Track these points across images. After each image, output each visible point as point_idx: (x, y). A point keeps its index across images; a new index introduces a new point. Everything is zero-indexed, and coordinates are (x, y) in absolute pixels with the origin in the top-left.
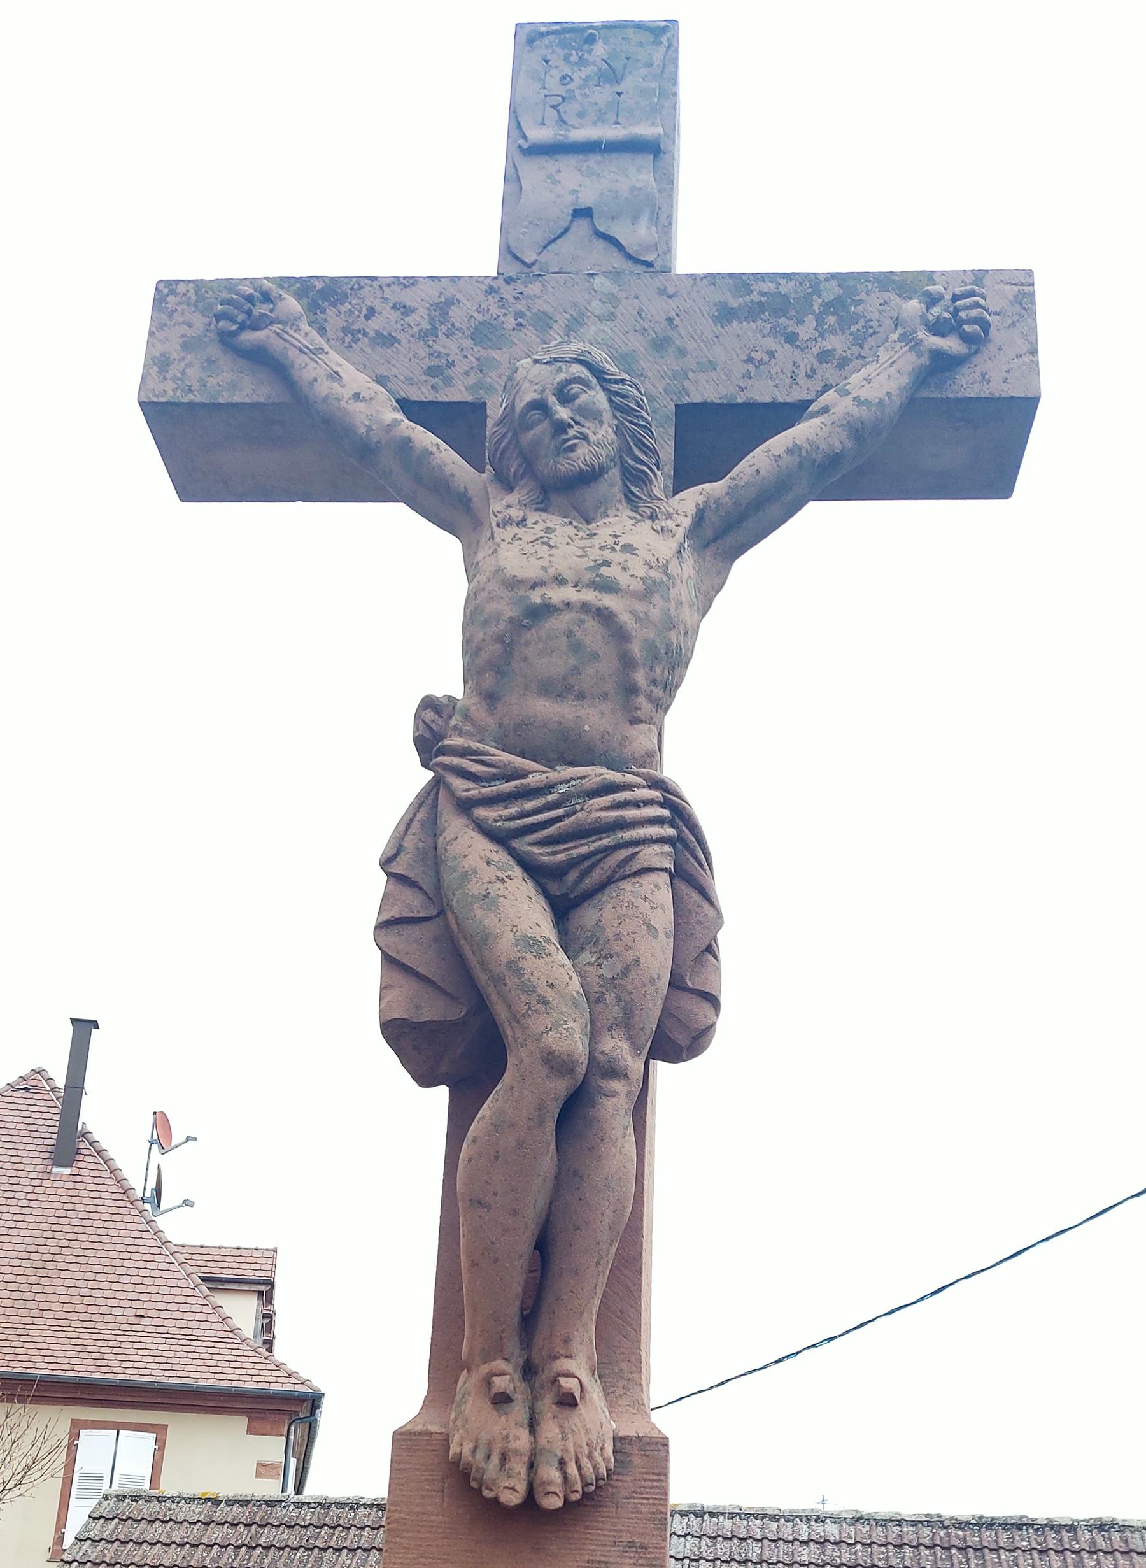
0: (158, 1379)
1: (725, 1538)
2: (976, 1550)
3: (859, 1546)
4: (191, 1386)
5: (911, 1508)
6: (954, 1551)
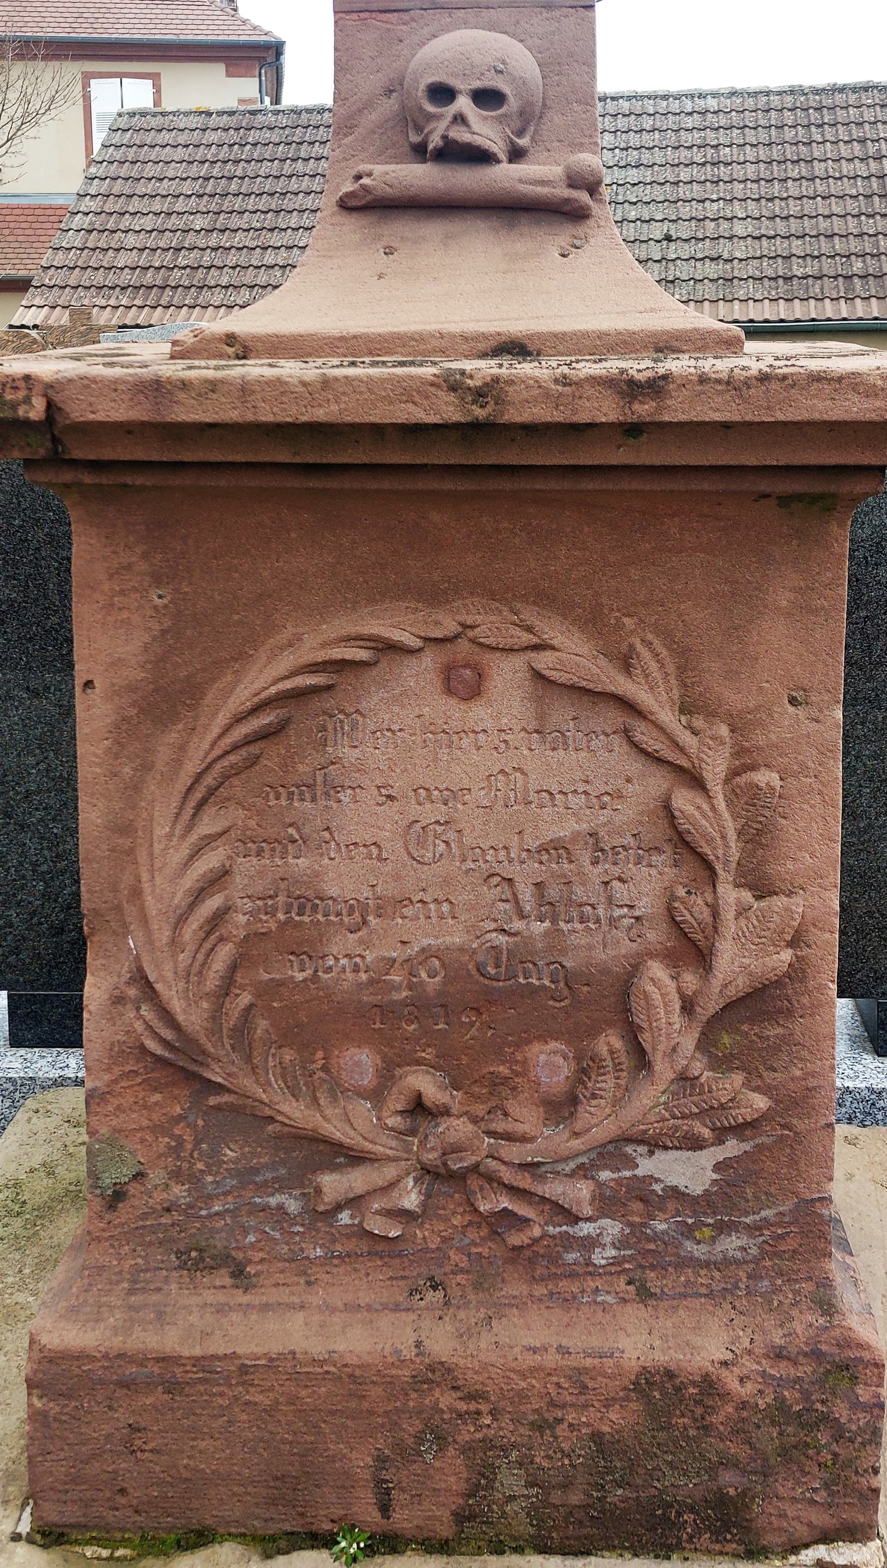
0: (146, 37)
1: (624, 116)
2: (829, 109)
3: (734, 113)
4: (175, 41)
5: (776, 82)
6: (811, 111)
